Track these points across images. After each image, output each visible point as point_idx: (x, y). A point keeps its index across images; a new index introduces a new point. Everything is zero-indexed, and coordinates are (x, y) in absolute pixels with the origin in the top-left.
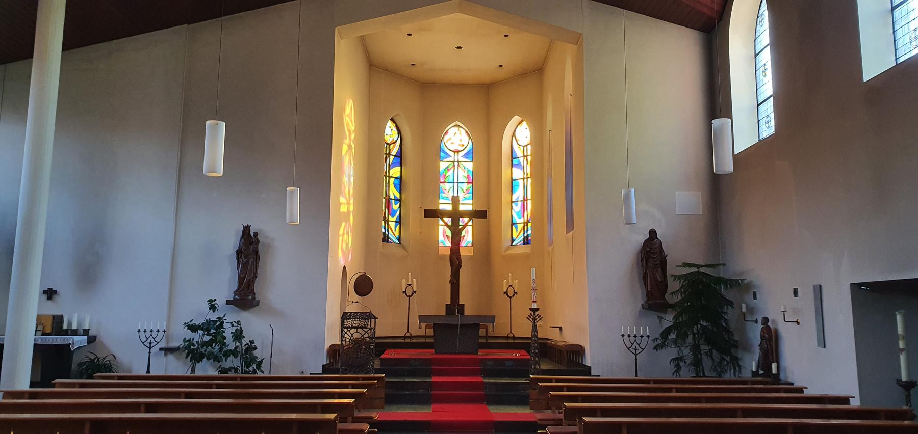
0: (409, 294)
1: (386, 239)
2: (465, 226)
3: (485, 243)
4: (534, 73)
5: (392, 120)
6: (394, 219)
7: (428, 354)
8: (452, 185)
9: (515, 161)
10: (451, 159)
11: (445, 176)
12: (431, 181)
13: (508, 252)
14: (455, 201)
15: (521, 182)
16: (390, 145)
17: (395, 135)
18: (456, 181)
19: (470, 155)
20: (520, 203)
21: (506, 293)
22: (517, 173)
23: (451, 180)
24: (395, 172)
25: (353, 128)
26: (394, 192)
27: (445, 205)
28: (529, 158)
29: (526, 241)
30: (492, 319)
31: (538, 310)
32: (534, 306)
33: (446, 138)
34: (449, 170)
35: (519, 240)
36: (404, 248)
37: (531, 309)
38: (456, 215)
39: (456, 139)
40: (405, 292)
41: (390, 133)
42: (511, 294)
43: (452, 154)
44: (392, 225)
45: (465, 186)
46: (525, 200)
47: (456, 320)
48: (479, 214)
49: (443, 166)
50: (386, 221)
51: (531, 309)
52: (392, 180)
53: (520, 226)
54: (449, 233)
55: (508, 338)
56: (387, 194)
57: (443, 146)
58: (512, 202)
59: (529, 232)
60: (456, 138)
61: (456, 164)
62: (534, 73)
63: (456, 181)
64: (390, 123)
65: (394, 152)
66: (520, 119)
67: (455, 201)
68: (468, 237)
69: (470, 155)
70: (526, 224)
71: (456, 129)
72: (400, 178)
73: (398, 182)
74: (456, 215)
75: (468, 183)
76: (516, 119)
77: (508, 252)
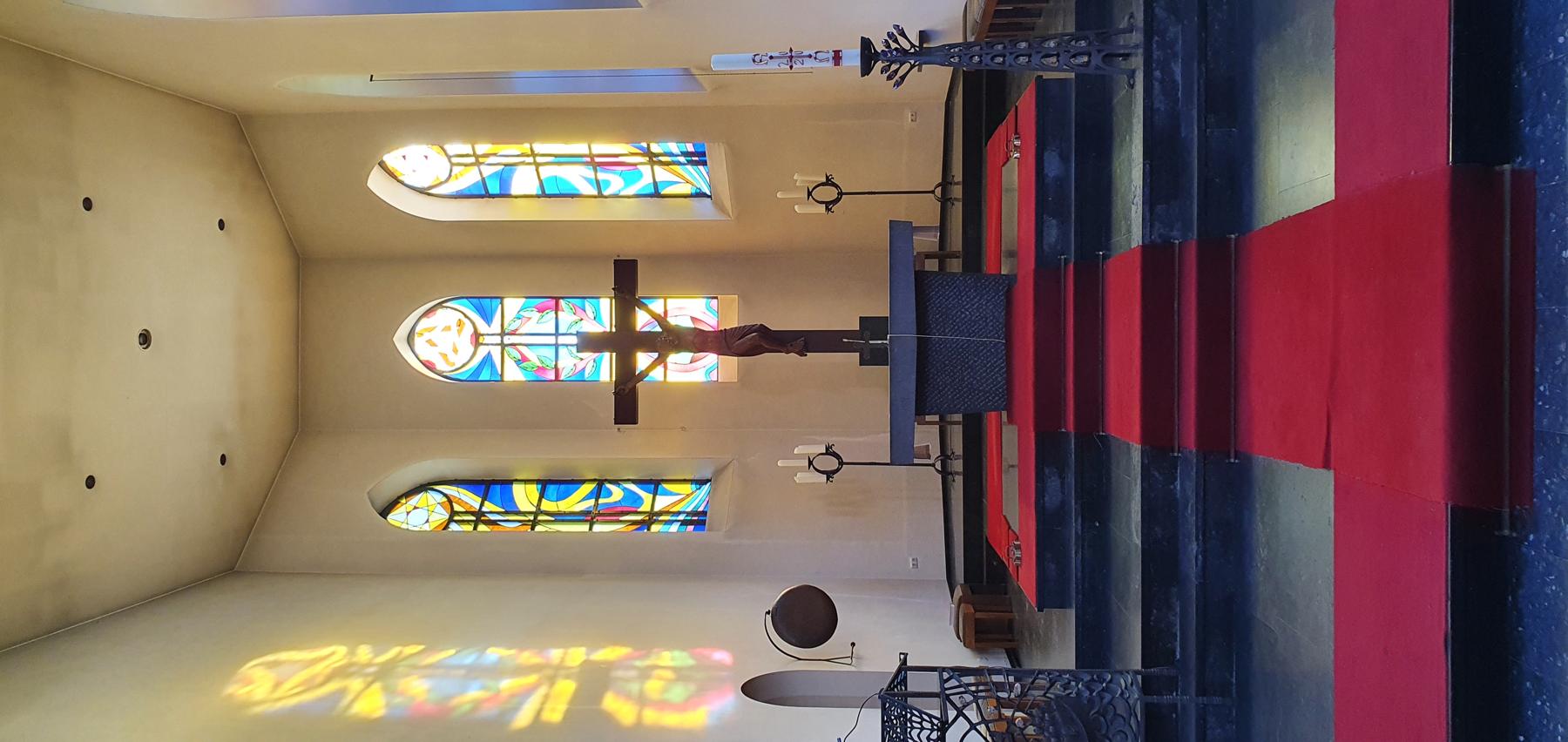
0: (833, 464)
1: (698, 520)
2: (661, 320)
3: (700, 264)
4: (243, 139)
5: (385, 513)
6: (647, 497)
7: (1011, 444)
8: (562, 350)
9: (494, 188)
10: (496, 353)
11: (541, 369)
12: (546, 403)
13: (728, 204)
14: (590, 343)
15: (546, 172)
16: (453, 513)
17: (430, 499)
18: (552, 340)
19: (484, 305)
20: (602, 176)
21: (829, 205)
22: (524, 181)
23: (551, 352)
24: (525, 497)
25: (341, 650)
26: (578, 500)
27: (603, 368)
28: (482, 148)
29: (698, 158)
30: (900, 231)
31: (866, 44)
32: (853, 59)
33: (441, 366)
34: (524, 359)
35: (697, 178)
36: (719, 472)
37: (866, 69)
38: (623, 341)
39: (446, 341)
40: (829, 474)
41: (420, 515)
42: (831, 193)
43: (482, 351)
44: (662, 502)
45: (566, 317)
46: (593, 162)
47: (905, 338)
48: (626, 282)
49: (513, 374)
50: (652, 517)
51: (866, 69)
52: (547, 505)
53: (662, 174)
54: (673, 358)
55: (945, 201)
56: (588, 517)
57: (464, 374)
58: (600, 195)
59: (673, 147)
60: (439, 340)
61: (507, 340)
62: (243, 139)
63: (552, 340)
64: (396, 517)
65: (473, 501)
66: (377, 169)
67: (590, 343)
68: (690, 310)
69: (484, 305)
70: (652, 158)
71: (419, 342)
72: (544, 484)
73: (551, 489)
74: (623, 341)
75: (557, 309)
76: (377, 183)
77: (728, 204)
